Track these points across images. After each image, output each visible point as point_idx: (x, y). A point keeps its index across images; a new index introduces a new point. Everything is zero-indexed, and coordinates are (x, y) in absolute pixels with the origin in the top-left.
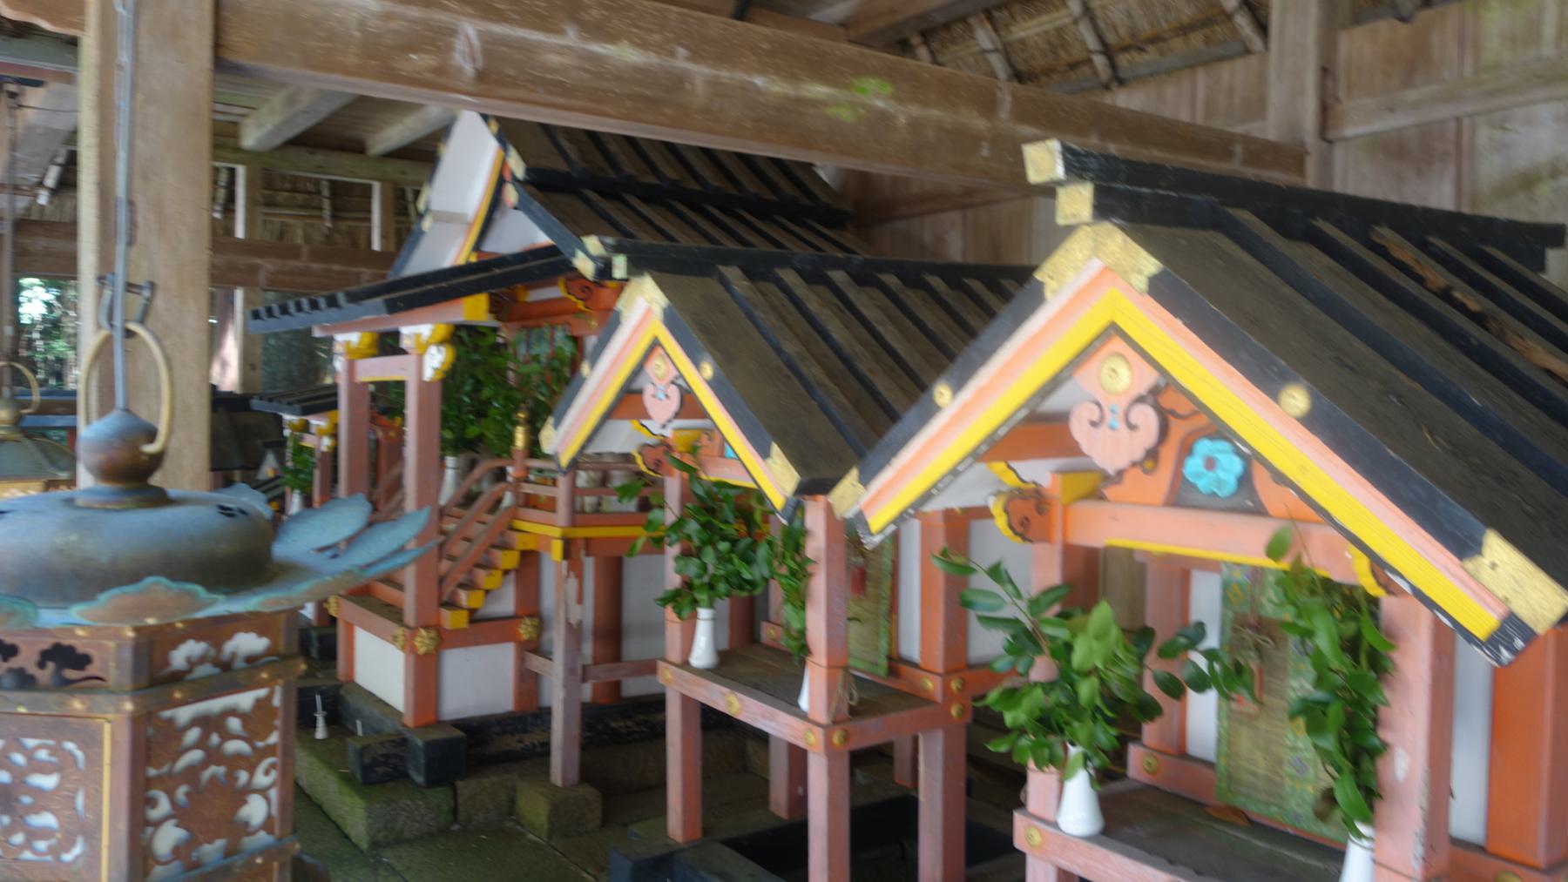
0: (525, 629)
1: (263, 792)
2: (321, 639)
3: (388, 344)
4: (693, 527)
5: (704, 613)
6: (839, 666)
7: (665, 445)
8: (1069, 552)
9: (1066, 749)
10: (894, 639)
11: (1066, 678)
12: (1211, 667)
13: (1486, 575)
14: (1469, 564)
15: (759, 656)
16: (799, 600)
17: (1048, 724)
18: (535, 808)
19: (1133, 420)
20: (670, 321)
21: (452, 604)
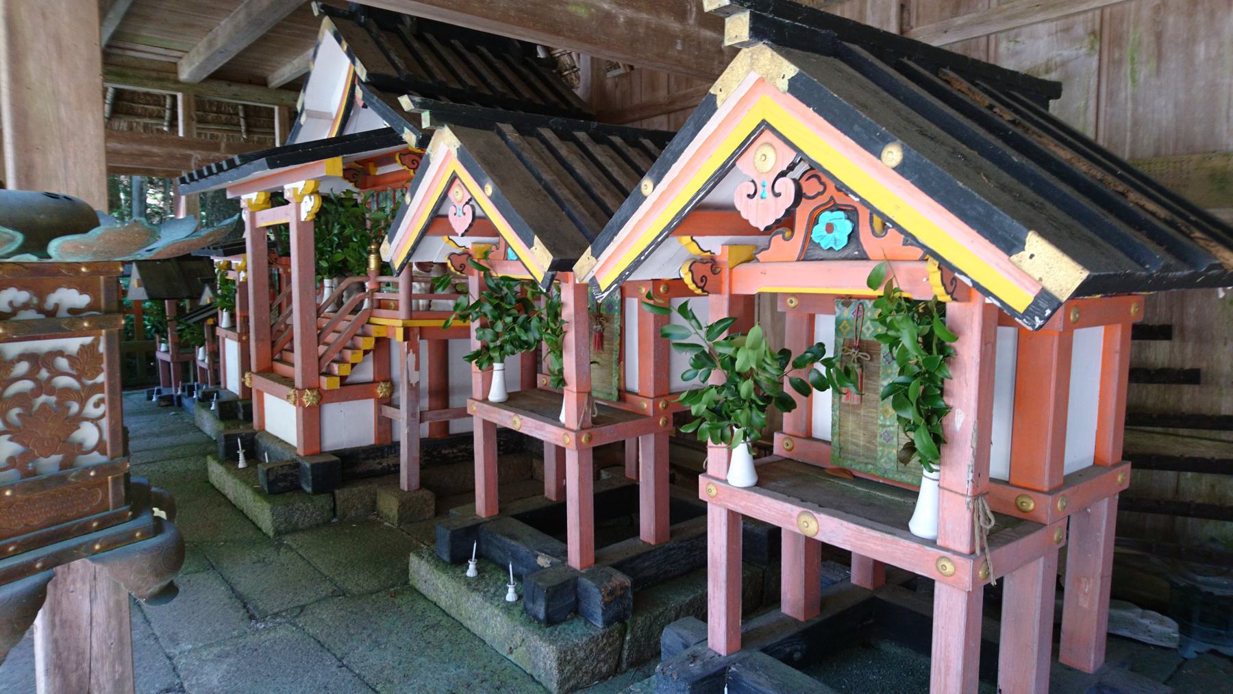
0: (382, 389)
1: (95, 421)
2: (244, 407)
3: (277, 199)
4: (487, 308)
5: (497, 366)
6: (585, 393)
7: (467, 253)
8: (734, 299)
9: (732, 431)
10: (622, 378)
11: (732, 383)
12: (828, 372)
13: (1027, 264)
14: (1014, 258)
15: (535, 394)
16: (558, 350)
17: (719, 413)
18: (389, 505)
19: (777, 190)
20: (462, 158)
21: (329, 374)
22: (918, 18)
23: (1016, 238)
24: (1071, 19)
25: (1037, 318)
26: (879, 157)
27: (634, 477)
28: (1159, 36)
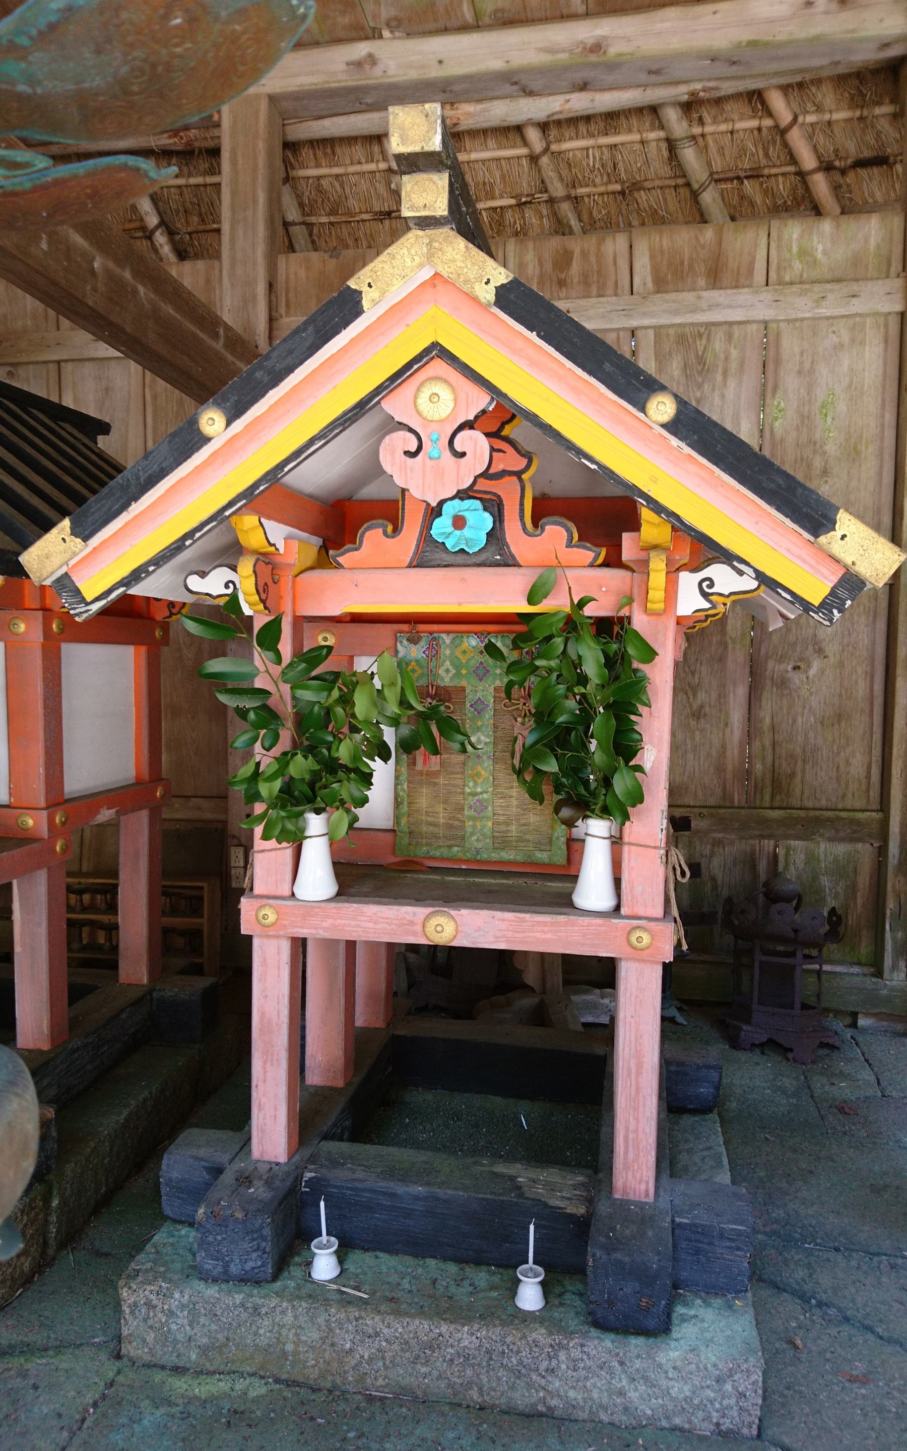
14: (823, 539)
19: (458, 447)
22: (288, 305)
23: (824, 516)
25: (835, 611)
26: (643, 409)
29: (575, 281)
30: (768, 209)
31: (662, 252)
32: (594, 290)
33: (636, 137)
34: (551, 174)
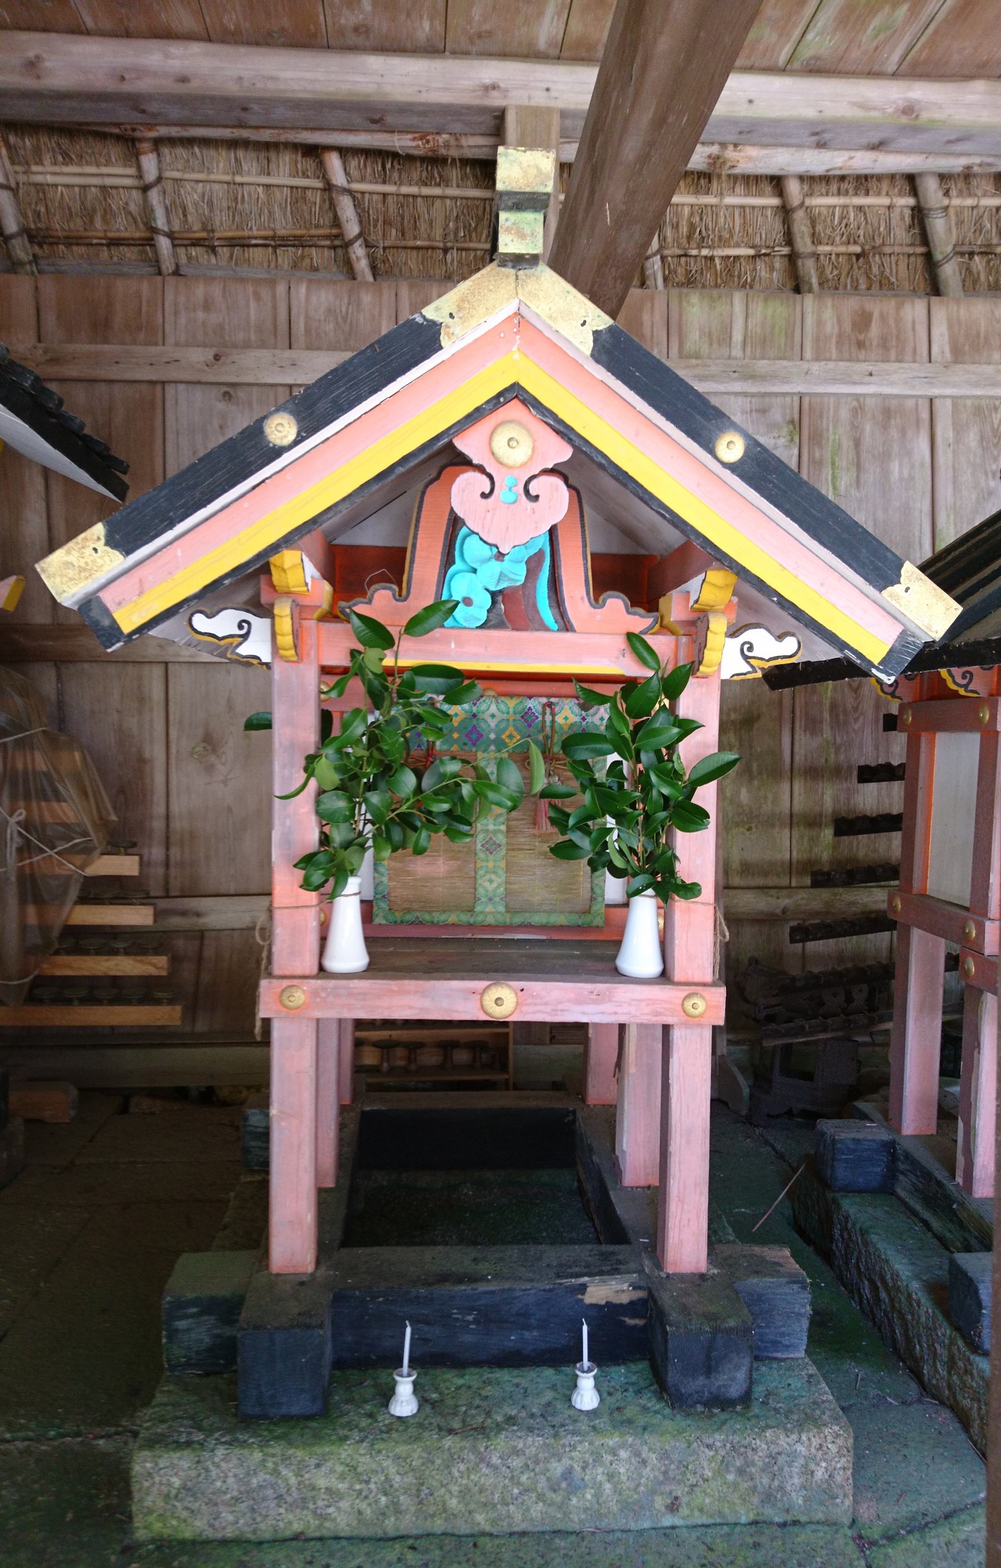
24: (767, 399)
27: (182, 450)
28: (857, 443)
29: (875, 343)
30: (989, 285)
31: (959, 323)
32: (893, 355)
33: (885, 201)
34: (803, 228)
